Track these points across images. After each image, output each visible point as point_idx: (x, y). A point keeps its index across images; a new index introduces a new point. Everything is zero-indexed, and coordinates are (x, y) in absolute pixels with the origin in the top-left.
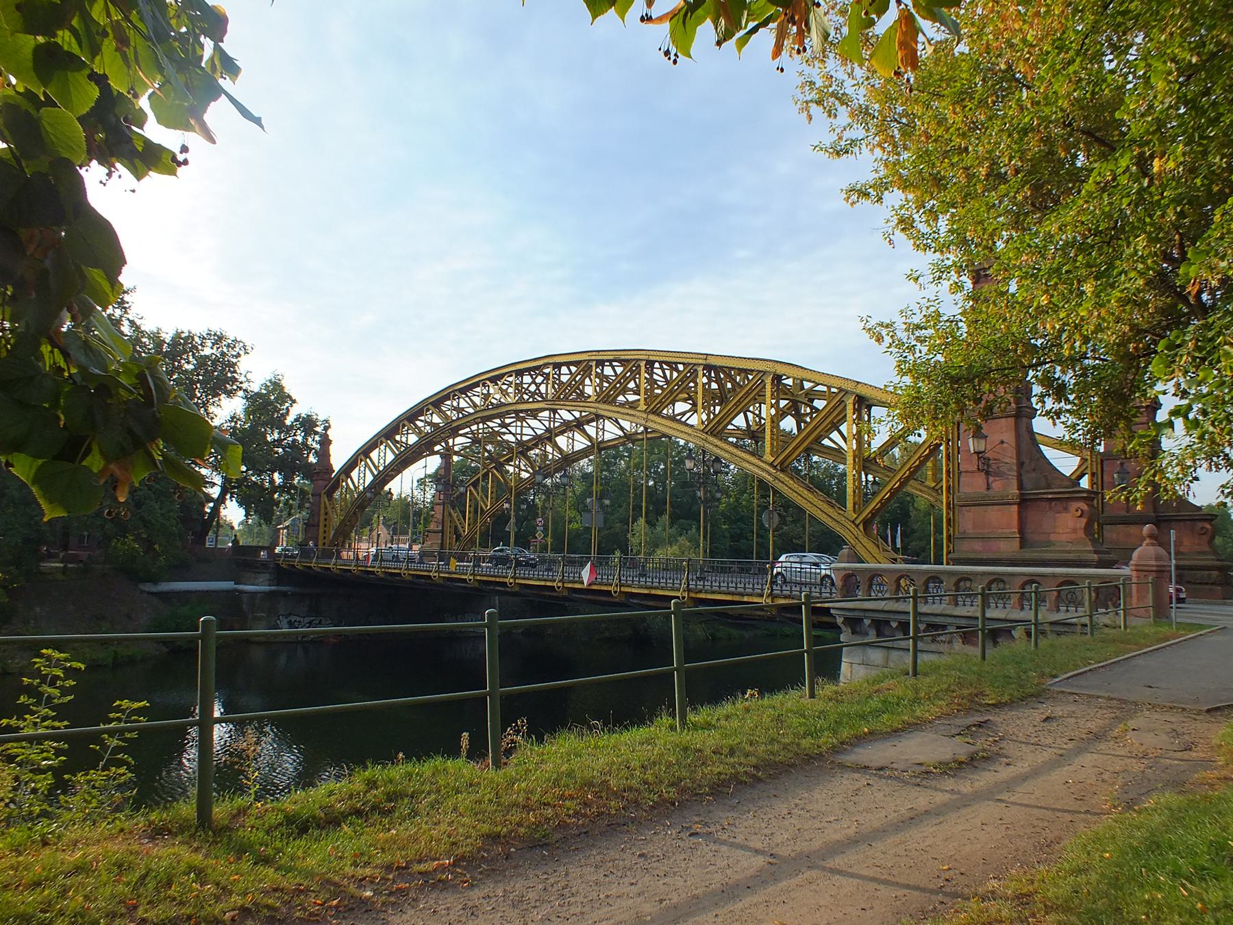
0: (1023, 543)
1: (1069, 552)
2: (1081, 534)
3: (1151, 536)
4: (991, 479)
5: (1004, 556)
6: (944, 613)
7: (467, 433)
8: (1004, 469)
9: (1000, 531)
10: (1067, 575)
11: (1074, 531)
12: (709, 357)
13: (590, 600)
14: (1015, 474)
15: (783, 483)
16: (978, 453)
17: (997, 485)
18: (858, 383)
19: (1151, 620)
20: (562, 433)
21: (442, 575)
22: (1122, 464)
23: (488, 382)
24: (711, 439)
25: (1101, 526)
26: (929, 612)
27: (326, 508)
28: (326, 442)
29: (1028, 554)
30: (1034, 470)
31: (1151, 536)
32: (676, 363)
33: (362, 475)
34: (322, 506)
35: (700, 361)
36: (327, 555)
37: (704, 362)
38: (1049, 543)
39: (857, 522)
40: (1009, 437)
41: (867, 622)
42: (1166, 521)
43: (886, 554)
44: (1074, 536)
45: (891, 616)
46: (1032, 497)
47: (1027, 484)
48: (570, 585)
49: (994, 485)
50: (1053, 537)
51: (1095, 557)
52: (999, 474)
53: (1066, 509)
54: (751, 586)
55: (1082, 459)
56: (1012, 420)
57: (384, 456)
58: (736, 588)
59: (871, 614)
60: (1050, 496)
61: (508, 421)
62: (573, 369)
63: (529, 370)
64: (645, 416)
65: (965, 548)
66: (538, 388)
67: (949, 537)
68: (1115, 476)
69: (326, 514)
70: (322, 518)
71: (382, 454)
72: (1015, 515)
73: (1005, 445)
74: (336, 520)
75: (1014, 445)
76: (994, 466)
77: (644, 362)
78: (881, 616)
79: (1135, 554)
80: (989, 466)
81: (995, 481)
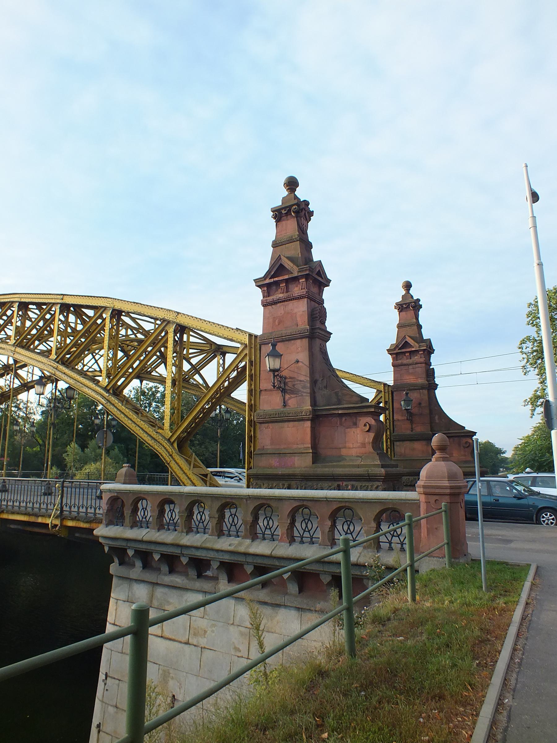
0: (316, 458)
1: (358, 466)
2: (369, 448)
3: (442, 448)
4: (287, 396)
5: (297, 471)
6: (204, 546)
8: (299, 386)
9: (295, 446)
11: (363, 445)
12: (65, 297)
13: (352, 407)
14: (309, 391)
15: (113, 405)
16: (273, 371)
17: (292, 402)
18: (178, 313)
19: (446, 559)
22: (407, 394)
24: (61, 367)
25: (393, 441)
26: (188, 544)
29: (321, 470)
30: (326, 387)
31: (442, 448)
35: (58, 301)
37: (60, 301)
38: (340, 458)
39: (172, 440)
40: (303, 356)
43: (197, 470)
44: (363, 450)
45: (152, 547)
46: (324, 413)
47: (319, 399)
49: (289, 402)
50: (344, 452)
51: (383, 471)
52: (294, 392)
53: (355, 424)
55: (377, 390)
56: (305, 342)
60: (340, 412)
64: (13, 349)
67: (250, 453)
68: (402, 403)
72: (309, 431)
73: (300, 364)
75: (307, 364)
76: (290, 384)
77: (17, 304)
78: (143, 547)
79: (423, 473)
80: (285, 384)
81: (290, 399)
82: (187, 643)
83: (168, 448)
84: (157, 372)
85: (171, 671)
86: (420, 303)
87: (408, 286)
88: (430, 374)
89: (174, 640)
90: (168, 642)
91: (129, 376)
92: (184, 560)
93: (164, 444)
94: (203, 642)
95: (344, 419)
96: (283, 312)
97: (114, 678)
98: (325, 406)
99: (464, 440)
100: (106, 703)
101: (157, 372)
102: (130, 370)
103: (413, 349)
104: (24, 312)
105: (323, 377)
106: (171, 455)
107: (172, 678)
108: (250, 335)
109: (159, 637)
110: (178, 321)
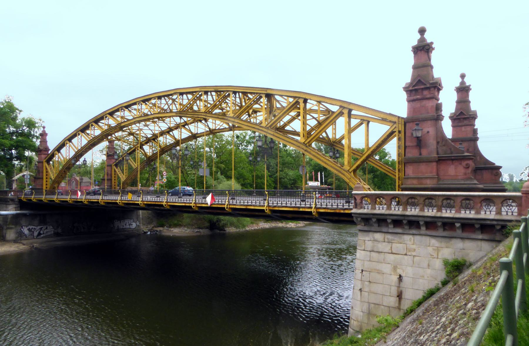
7: (126, 130)
10: (411, 195)
20: (146, 143)
21: (123, 202)
23: (142, 103)
27: (46, 169)
28: (44, 135)
30: (444, 145)
32: (247, 93)
33: (68, 151)
34: (44, 168)
36: (52, 192)
37: (265, 92)
39: (350, 171)
41: (374, 220)
42: (480, 169)
48: (199, 205)
54: (243, 201)
57: (81, 141)
58: (252, 203)
59: (376, 216)
60: (453, 158)
61: (148, 123)
62: (190, 96)
63: (164, 96)
65: (409, 183)
66: (169, 106)
69: (47, 172)
70: (45, 174)
71: (80, 140)
74: (53, 175)
82: (406, 255)
85: (398, 266)
87: (463, 76)
88: (475, 132)
89: (398, 254)
90: (395, 255)
91: (186, 107)
92: (405, 222)
94: (414, 254)
95: (454, 162)
96: (419, 106)
97: (367, 271)
98: (443, 155)
99: (494, 172)
100: (363, 281)
103: (466, 117)
105: (443, 140)
107: (399, 268)
108: (399, 117)
109: (390, 253)
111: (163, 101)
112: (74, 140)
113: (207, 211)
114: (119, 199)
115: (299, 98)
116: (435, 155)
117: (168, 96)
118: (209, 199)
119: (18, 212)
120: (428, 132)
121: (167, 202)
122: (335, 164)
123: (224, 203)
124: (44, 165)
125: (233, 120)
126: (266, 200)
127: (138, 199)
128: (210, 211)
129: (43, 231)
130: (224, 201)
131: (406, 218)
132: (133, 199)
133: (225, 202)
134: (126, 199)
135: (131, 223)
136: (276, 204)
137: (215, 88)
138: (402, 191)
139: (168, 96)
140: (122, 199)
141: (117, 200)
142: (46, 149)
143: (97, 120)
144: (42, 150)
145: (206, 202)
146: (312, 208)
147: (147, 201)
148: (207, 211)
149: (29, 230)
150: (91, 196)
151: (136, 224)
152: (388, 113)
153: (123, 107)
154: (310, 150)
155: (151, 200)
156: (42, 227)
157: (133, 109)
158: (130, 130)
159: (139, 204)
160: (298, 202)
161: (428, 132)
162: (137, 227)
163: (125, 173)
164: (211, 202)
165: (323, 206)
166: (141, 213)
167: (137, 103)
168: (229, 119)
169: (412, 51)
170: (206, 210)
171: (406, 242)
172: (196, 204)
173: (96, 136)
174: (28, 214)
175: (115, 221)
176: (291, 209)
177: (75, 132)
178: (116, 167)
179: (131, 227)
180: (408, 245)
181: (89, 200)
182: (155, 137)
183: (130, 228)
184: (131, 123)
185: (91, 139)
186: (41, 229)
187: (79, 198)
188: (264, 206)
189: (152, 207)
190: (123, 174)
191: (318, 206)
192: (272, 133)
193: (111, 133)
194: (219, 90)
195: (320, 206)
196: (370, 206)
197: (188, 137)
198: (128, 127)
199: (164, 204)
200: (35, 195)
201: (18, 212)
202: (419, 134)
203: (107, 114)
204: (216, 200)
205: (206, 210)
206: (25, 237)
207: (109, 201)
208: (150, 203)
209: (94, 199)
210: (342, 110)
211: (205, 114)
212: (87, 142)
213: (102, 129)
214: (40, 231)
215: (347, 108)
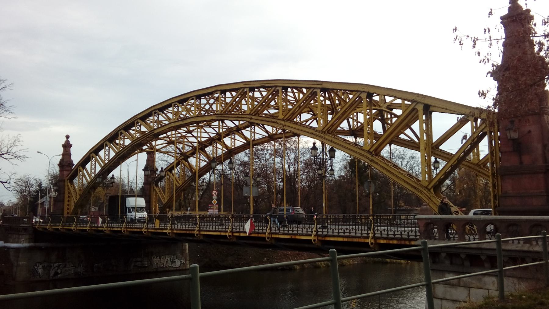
23: (178, 104)
27: (69, 189)
34: (66, 188)
39: (429, 187)
41: (443, 255)
62: (234, 94)
69: (69, 193)
71: (107, 153)
74: (75, 199)
83: (426, 193)
84: (340, 127)
86: (531, 13)
87: (68, 137)
91: (231, 105)
93: (423, 190)
101: (340, 127)
102: (234, 103)
104: (328, 106)
106: (429, 198)
110: (426, 102)
111: (204, 101)
112: (101, 153)
113: (287, 244)
114: (168, 228)
115: (361, 92)
116: (540, 163)
117: (208, 94)
118: (247, 226)
119: (31, 244)
120: (530, 132)
121: (199, 231)
122: (408, 178)
123: (310, 233)
124: (66, 184)
125: (283, 122)
126: (370, 229)
127: (194, 228)
128: (251, 242)
129: (61, 270)
130: (310, 230)
131: (485, 252)
132: (161, 227)
133: (312, 232)
134: (153, 227)
135: (174, 260)
136: (326, 233)
137: (261, 83)
138: (499, 215)
139: (208, 94)
140: (149, 227)
141: (142, 228)
142: (69, 164)
143: (127, 127)
144: (64, 166)
145: (244, 230)
146: (195, 230)
147: (177, 230)
148: (287, 244)
149: (43, 268)
150: (350, 225)
151: (181, 262)
152: (475, 107)
153: (156, 109)
154: (376, 161)
155: (181, 228)
156: (60, 265)
157: (169, 113)
158: (169, 138)
159: (86, 230)
160: (359, 230)
161: (530, 132)
162: (182, 266)
163: (166, 195)
164: (250, 230)
165: (383, 236)
166: (187, 247)
167: (173, 105)
168: (278, 121)
169: (501, 23)
170: (246, 241)
171: (487, 287)
172: (76, 227)
173: (126, 146)
174: (43, 247)
175: (153, 258)
176: (345, 240)
177: (102, 142)
178: (70, 182)
179: (173, 265)
180: (490, 291)
181: (112, 229)
182: (202, 146)
183: (172, 267)
184: (165, 130)
185: (120, 151)
186: (58, 267)
187: (100, 226)
188: (368, 238)
189: (184, 238)
190: (165, 193)
191: (377, 235)
192: (330, 139)
193: (142, 142)
194: (267, 85)
195: (379, 236)
196: (457, 236)
197: (244, 144)
198: (166, 133)
199: (195, 233)
200: (51, 223)
201: (31, 244)
202: (515, 135)
203: (139, 118)
204: (256, 228)
205: (246, 241)
206: (38, 277)
207: (133, 230)
208: (179, 232)
209: (117, 228)
210: (416, 105)
211: (250, 116)
212: (115, 154)
213: (133, 137)
214: (57, 270)
215: (421, 103)
